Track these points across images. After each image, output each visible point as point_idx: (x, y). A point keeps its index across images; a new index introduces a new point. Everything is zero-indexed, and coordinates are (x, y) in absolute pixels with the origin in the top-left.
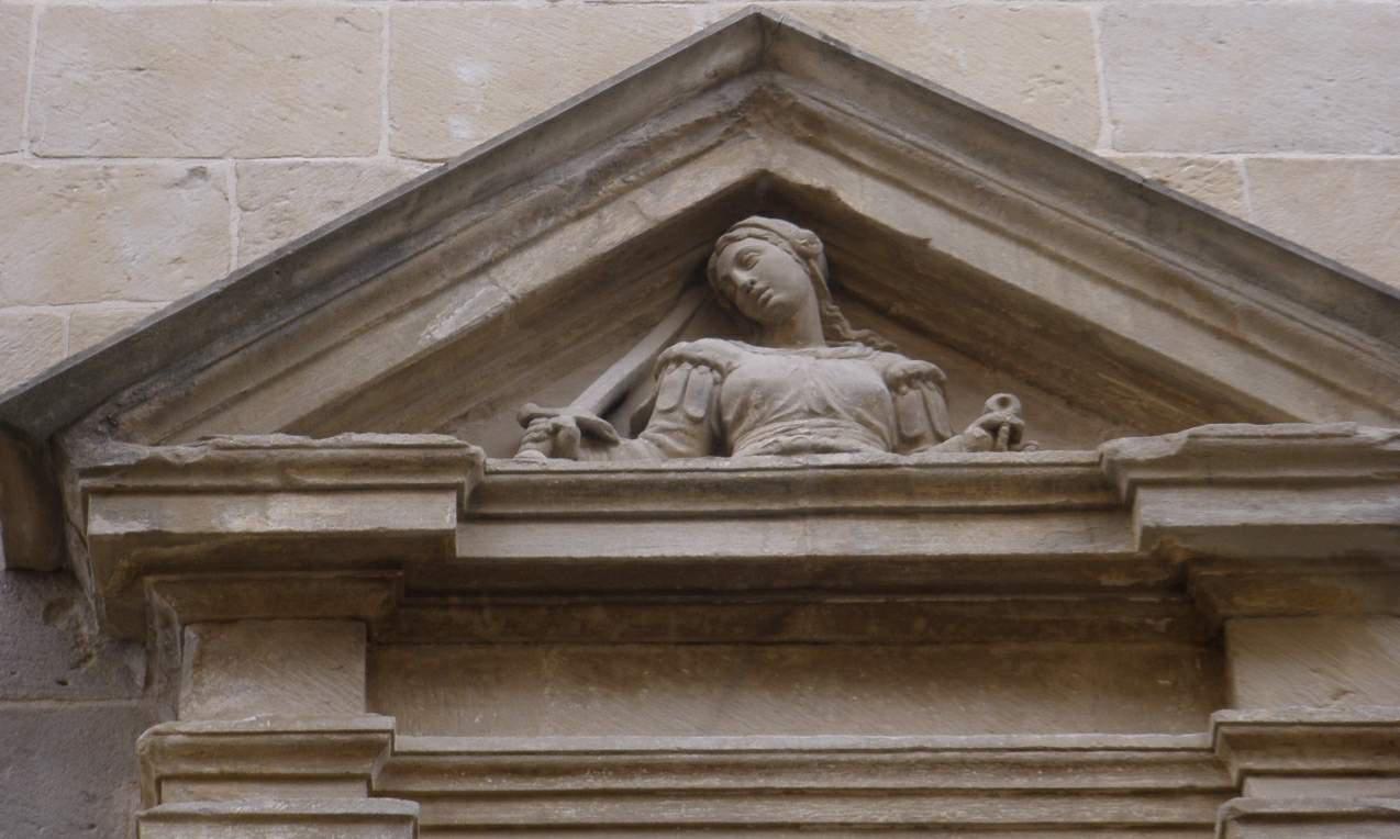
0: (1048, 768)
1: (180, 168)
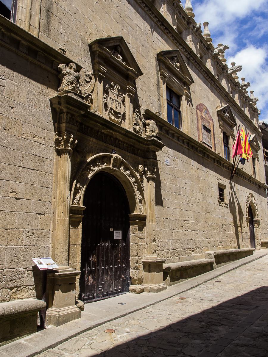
1: (94, 24)
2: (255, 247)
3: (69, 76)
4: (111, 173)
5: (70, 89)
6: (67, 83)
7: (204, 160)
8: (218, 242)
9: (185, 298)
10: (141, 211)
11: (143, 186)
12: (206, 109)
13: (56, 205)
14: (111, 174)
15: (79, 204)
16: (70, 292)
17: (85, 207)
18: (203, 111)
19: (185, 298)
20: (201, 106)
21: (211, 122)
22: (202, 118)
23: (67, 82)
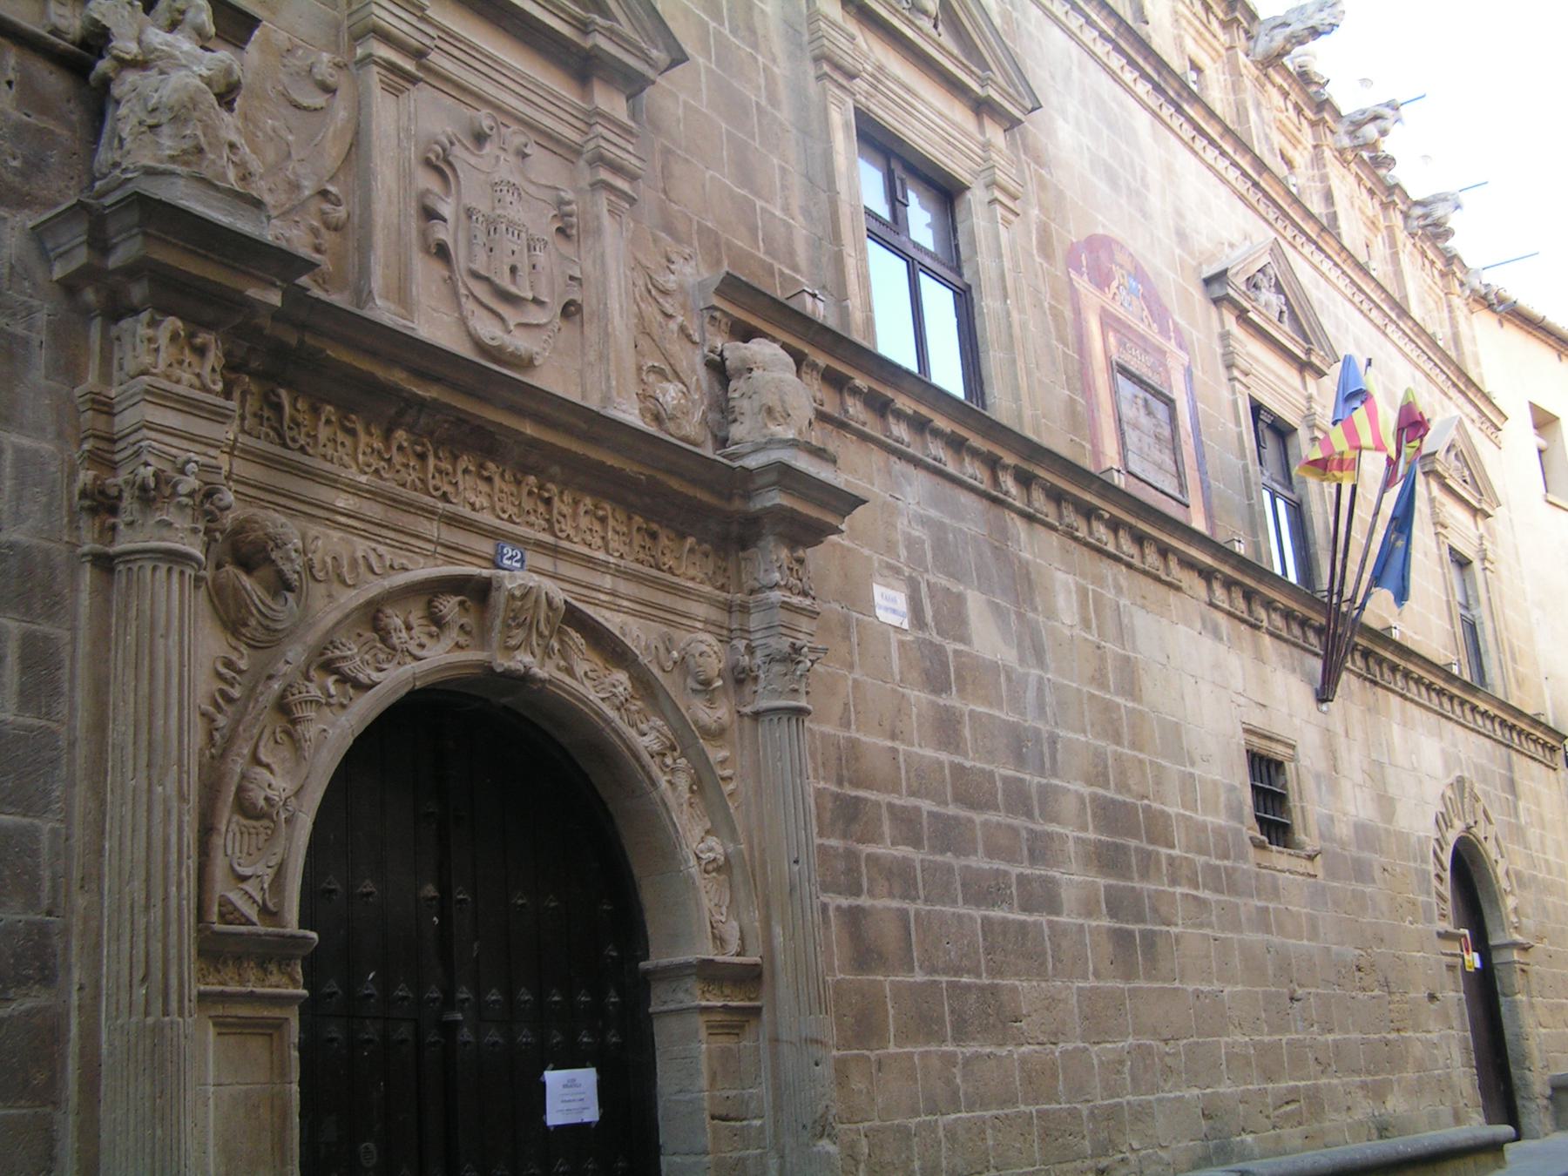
0: (487, 56)
2: (1512, 1117)
3: (162, 72)
4: (504, 701)
5: (172, 159)
6: (151, 121)
7: (891, 419)
8: (1267, 1106)
9: (1283, 156)
10: (719, 940)
11: (727, 773)
12: (1129, 266)
13: (100, 935)
14: (505, 707)
15: (269, 914)
16: (1430, 433)
17: (314, 935)
18: (1115, 284)
19: (1283, 156)
20: (1103, 256)
21: (1171, 346)
22: (1109, 321)
23: (143, 116)
